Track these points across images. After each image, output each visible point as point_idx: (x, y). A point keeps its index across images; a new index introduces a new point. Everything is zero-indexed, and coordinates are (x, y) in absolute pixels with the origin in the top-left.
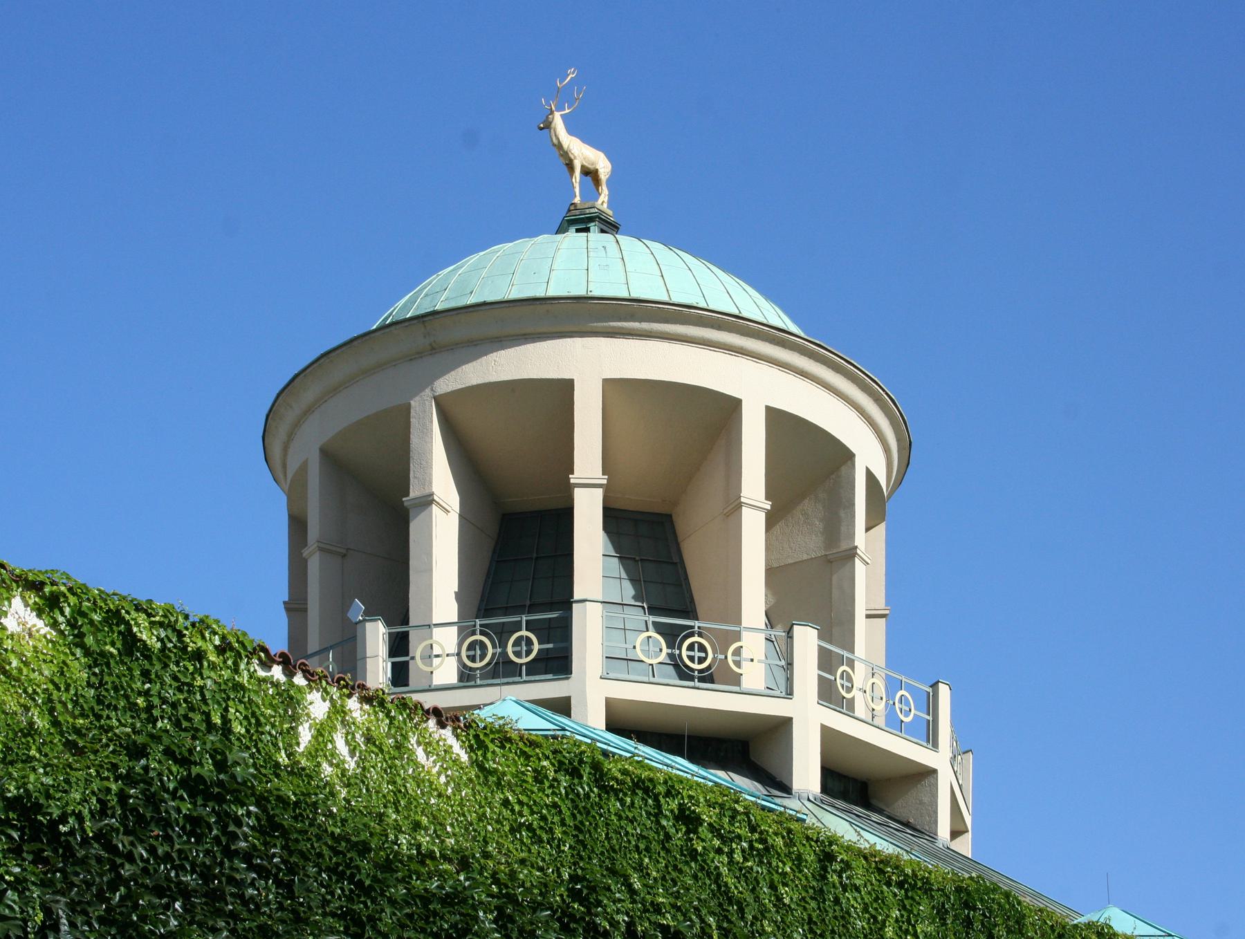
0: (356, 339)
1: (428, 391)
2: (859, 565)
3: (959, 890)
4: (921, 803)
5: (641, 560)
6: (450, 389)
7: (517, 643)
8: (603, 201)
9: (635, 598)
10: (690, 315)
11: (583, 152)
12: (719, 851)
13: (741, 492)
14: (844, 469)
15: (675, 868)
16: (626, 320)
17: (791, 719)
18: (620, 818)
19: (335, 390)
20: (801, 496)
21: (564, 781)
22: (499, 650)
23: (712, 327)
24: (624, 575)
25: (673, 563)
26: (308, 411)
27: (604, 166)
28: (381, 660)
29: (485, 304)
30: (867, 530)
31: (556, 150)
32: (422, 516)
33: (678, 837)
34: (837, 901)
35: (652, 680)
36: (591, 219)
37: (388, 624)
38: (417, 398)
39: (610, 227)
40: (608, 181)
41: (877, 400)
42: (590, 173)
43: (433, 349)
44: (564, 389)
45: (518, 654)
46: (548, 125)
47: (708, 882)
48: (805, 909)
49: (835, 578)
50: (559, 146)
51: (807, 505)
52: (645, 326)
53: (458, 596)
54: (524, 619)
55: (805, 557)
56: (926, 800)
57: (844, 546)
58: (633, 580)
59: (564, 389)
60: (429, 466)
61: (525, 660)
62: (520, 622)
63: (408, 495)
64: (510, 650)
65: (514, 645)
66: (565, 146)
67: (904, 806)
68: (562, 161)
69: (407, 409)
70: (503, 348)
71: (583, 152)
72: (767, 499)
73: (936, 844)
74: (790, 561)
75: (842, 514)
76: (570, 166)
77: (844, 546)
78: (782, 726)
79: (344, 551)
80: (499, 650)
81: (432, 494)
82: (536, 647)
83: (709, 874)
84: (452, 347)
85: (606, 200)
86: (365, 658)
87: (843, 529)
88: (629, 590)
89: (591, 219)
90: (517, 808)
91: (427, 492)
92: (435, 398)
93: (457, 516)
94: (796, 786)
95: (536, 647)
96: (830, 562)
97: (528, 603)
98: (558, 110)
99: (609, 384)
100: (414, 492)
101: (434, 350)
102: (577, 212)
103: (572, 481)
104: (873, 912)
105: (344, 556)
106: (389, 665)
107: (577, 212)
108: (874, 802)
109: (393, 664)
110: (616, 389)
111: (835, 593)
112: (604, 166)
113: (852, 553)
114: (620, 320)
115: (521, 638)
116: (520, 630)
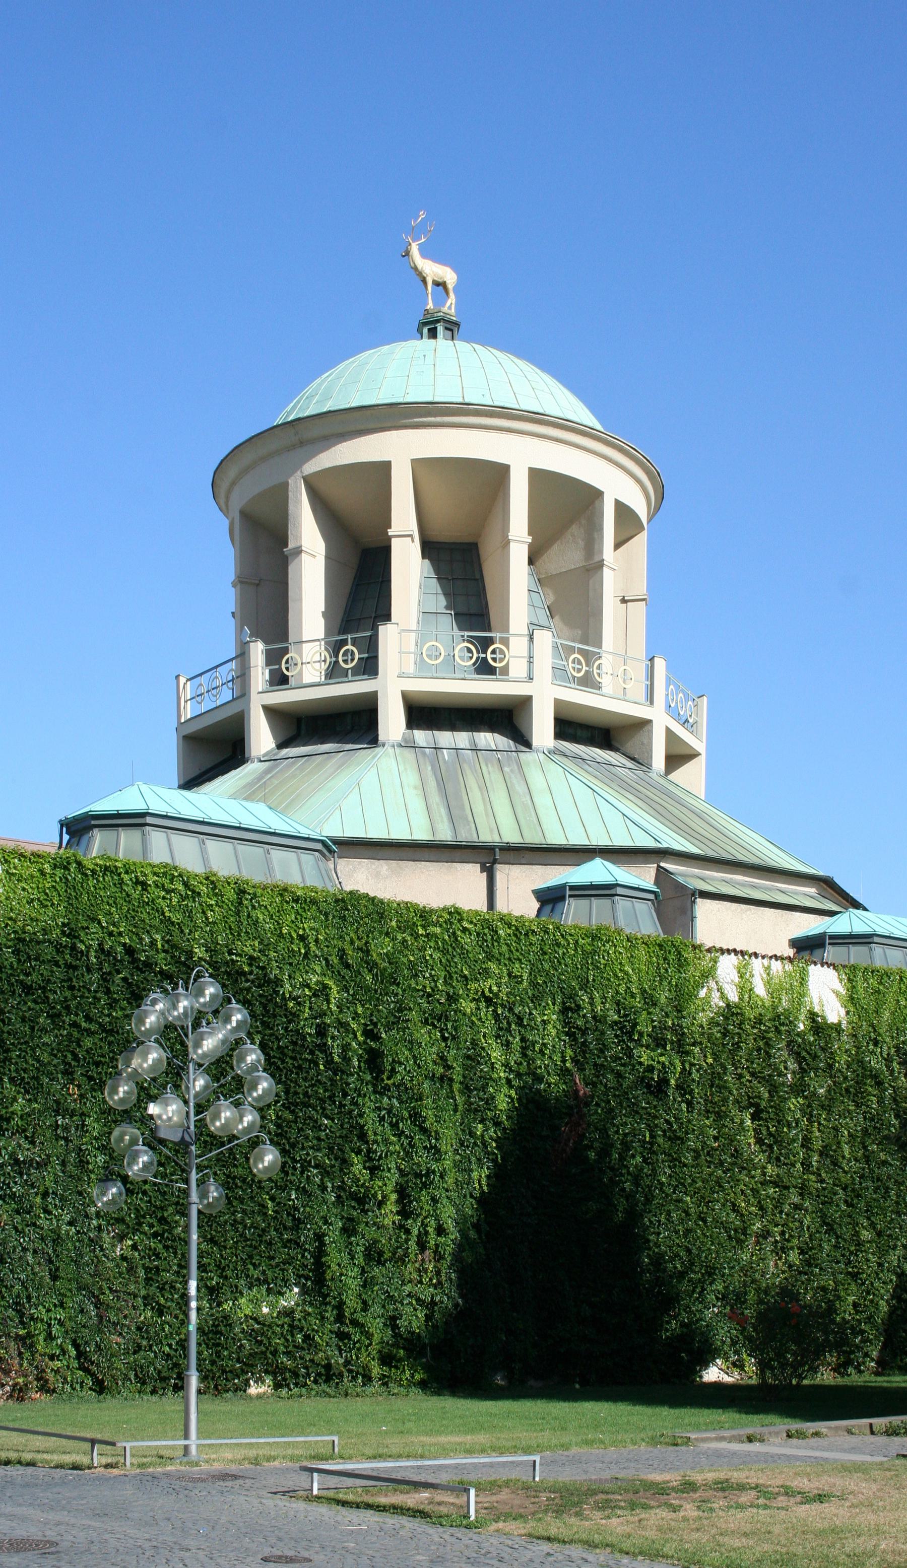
0: (253, 437)
1: (299, 472)
2: (607, 573)
3: (337, 901)
4: (643, 744)
5: (453, 579)
6: (312, 471)
7: (345, 654)
8: (450, 307)
9: (447, 608)
10: (470, 410)
11: (432, 269)
12: (164, 898)
13: (509, 531)
14: (597, 502)
15: (134, 910)
16: (425, 416)
17: (531, 697)
18: (96, 889)
19: (263, 459)
20: (571, 522)
21: (59, 872)
22: (334, 659)
23: (486, 416)
24: (440, 591)
25: (477, 580)
26: (233, 483)
27: (450, 277)
28: (260, 669)
29: (330, 412)
30: (617, 546)
31: (413, 271)
32: (296, 560)
33: (136, 895)
34: (249, 916)
35: (435, 675)
36: (438, 321)
37: (266, 642)
38: (292, 478)
39: (452, 327)
40: (454, 288)
41: (621, 450)
42: (440, 284)
43: (301, 443)
44: (384, 468)
45: (345, 661)
46: (407, 254)
47: (157, 915)
48: (226, 922)
49: (591, 582)
50: (415, 268)
51: (575, 529)
52: (439, 419)
53: (325, 615)
54: (350, 637)
55: (573, 567)
56: (645, 741)
57: (597, 559)
58: (446, 594)
59: (384, 468)
60: (299, 527)
61: (350, 665)
62: (347, 639)
63: (287, 546)
64: (340, 659)
65: (343, 655)
66: (419, 268)
67: (631, 746)
68: (418, 279)
69: (286, 485)
70: (345, 441)
71: (432, 269)
72: (529, 534)
73: (650, 774)
74: (564, 570)
75: (596, 535)
76: (424, 281)
77: (597, 559)
78: (526, 702)
79: (257, 582)
80: (334, 659)
81: (301, 547)
82: (357, 656)
83: (158, 911)
84: (313, 441)
85: (454, 302)
86: (250, 667)
87: (596, 547)
88: (442, 601)
89: (438, 321)
90: (30, 890)
91: (299, 544)
92: (304, 478)
93: (323, 558)
94: (535, 742)
95: (357, 656)
96: (588, 570)
97: (373, 615)
98: (414, 241)
99: (415, 462)
100: (291, 545)
101: (302, 443)
102: (429, 316)
103: (390, 534)
104: (277, 919)
105: (258, 585)
106: (267, 671)
107: (429, 316)
108: (614, 743)
109: (270, 670)
110: (420, 466)
111: (591, 594)
112: (450, 277)
113: (600, 565)
114: (421, 417)
115: (347, 650)
116: (347, 644)
